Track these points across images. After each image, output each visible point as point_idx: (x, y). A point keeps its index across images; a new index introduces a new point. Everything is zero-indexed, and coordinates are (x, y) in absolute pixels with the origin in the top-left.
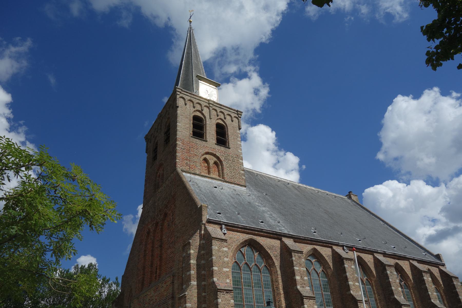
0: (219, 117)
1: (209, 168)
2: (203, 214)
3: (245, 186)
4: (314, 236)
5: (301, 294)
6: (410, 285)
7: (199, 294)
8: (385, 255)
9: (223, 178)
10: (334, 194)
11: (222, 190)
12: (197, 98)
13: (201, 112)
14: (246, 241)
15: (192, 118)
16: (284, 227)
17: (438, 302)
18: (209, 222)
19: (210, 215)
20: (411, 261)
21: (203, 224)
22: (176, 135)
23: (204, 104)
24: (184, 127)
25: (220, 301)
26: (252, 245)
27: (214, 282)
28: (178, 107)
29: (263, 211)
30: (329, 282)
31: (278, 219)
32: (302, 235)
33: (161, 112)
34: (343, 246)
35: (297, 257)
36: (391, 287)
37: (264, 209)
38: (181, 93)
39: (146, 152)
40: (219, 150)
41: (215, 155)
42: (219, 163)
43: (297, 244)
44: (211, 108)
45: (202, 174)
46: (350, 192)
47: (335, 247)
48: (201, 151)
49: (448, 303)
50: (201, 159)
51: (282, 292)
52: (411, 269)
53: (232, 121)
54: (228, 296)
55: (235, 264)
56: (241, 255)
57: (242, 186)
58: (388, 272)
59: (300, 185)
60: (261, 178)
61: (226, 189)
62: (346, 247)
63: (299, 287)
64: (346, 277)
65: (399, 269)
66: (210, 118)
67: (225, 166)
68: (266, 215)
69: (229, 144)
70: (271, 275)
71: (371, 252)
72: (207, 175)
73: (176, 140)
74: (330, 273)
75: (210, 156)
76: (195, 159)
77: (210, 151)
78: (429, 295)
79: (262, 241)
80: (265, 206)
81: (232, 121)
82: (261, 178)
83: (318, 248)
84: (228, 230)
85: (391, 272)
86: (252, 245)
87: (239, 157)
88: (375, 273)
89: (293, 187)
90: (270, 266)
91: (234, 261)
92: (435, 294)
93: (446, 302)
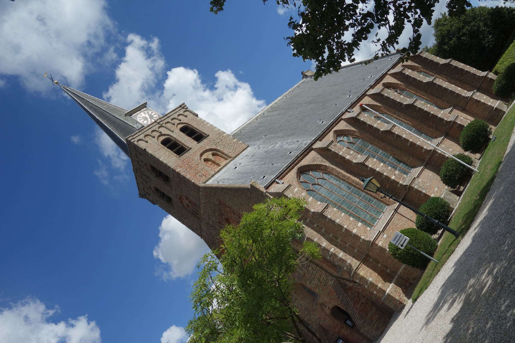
0: (176, 125)
1: (214, 162)
2: (258, 188)
3: (248, 146)
4: (325, 124)
5: (360, 163)
6: (404, 87)
7: (313, 228)
8: (372, 87)
9: (230, 158)
10: (296, 86)
11: (242, 165)
12: (147, 129)
13: (161, 135)
14: (297, 173)
15: (163, 146)
16: (304, 140)
17: (428, 78)
18: (267, 187)
19: (262, 184)
20: (389, 73)
21: (265, 193)
22: (169, 167)
23: (156, 128)
24: (167, 157)
25: (329, 217)
26: (303, 171)
27: (314, 212)
28: (145, 149)
29: (280, 146)
30: (364, 139)
31: (295, 140)
32: (320, 132)
33: (134, 167)
34: (346, 111)
35: (334, 147)
36: (396, 101)
37: (278, 145)
38: (133, 138)
39: (155, 204)
40: (205, 144)
41: (207, 151)
42: (215, 152)
43: (323, 140)
44: (164, 125)
45: (216, 170)
46: (302, 73)
47: (343, 117)
48: (196, 158)
49: (433, 72)
50: (203, 162)
51: (349, 175)
52: (394, 77)
53: (186, 116)
54: (330, 209)
55: (308, 192)
56: (304, 184)
57: (246, 148)
58: (386, 95)
59: (270, 105)
60: (245, 131)
61: (242, 161)
62: (348, 109)
63: (354, 161)
64: (369, 125)
65: (388, 86)
66: (173, 132)
67: (221, 150)
68: (286, 146)
69: (204, 134)
70: (332, 174)
71: (364, 95)
72: (220, 168)
73: (174, 171)
74: (357, 134)
75: (205, 155)
76: (200, 167)
77: (201, 151)
78: (419, 80)
79: (304, 162)
80: (276, 143)
81: (186, 116)
82: (245, 131)
83: (335, 128)
84: (281, 179)
85: (387, 93)
86: (303, 171)
87: (221, 133)
88: (379, 104)
89: (269, 112)
90: (325, 170)
91: (305, 191)
92: (421, 76)
93: (431, 73)
